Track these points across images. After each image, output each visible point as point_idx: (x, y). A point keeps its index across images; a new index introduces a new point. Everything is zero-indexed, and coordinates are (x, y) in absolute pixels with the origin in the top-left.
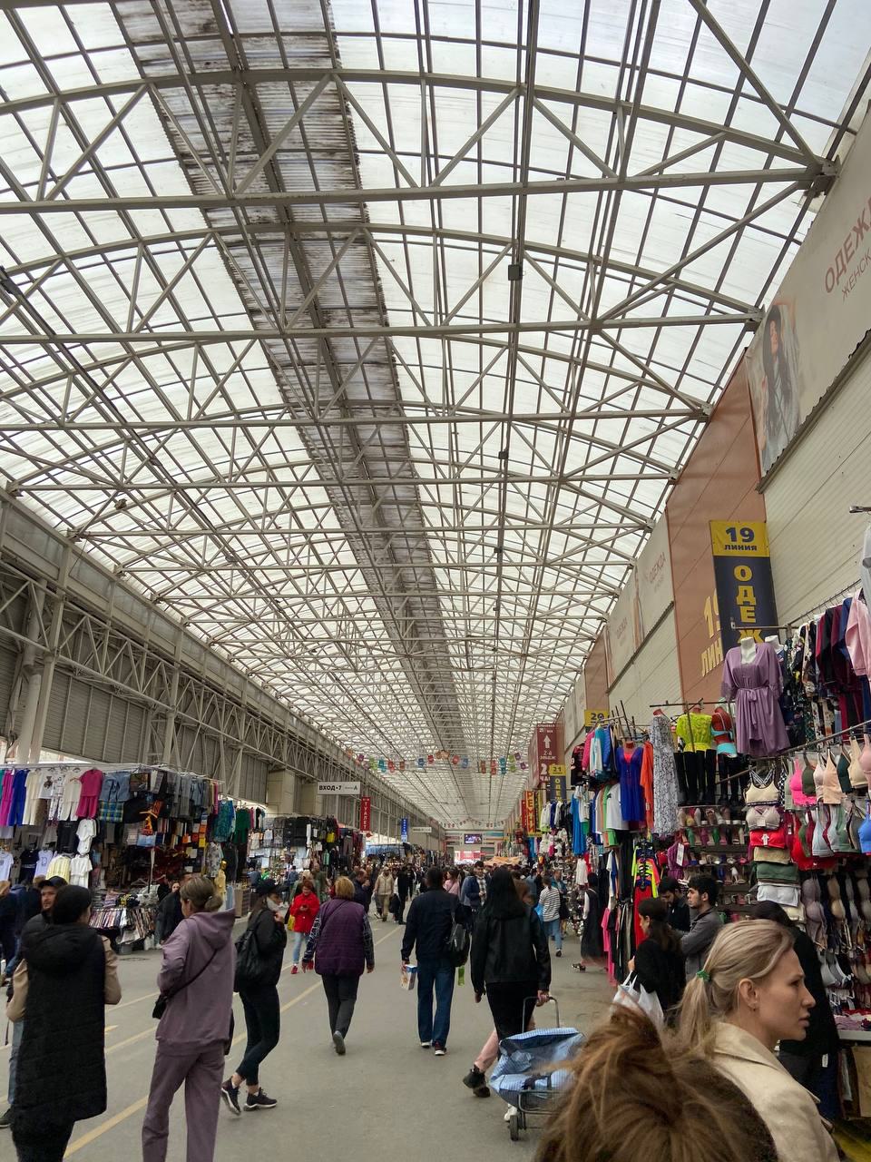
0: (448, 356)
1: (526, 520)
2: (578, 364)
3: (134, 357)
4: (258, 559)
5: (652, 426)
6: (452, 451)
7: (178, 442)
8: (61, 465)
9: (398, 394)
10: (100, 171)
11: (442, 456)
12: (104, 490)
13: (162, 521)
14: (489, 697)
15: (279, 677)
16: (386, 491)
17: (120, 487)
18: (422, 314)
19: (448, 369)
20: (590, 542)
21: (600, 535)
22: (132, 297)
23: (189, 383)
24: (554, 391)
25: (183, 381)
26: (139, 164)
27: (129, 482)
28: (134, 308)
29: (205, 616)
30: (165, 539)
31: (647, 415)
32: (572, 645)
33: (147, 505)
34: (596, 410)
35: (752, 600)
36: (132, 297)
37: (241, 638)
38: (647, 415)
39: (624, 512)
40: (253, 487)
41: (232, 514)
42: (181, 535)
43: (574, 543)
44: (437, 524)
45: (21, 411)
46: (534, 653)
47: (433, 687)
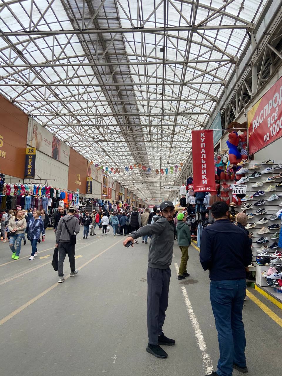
0: (143, 39)
1: (174, 81)
2: (189, 41)
3: (32, 40)
4: (86, 122)
5: (216, 65)
6: (143, 43)
7: (49, 70)
8: (7, 77)
9: (130, 72)
10: (85, 88)
11: (139, 52)
12: (23, 86)
13: (55, 109)
14: (159, 164)
15: (77, 143)
16: (116, 68)
17: (28, 85)
18: (143, 97)
19: (143, 43)
20: (195, 106)
21: (198, 103)
22: (30, 17)
23: (52, 48)
24: (180, 51)
25: (49, 47)
26: (59, 22)
27: (32, 83)
28: (31, 21)
29: (61, 132)
30: (44, 103)
31: (215, 61)
32: (187, 144)
33: (36, 90)
34: (196, 59)
35: (31, 161)
36: (30, 17)
37: (75, 140)
38: (215, 61)
39: (207, 94)
40: (62, 66)
41: (55, 78)
42: (50, 101)
43: (189, 105)
44: (140, 98)
45: (78, 138)
46: (174, 146)
47: (140, 157)
